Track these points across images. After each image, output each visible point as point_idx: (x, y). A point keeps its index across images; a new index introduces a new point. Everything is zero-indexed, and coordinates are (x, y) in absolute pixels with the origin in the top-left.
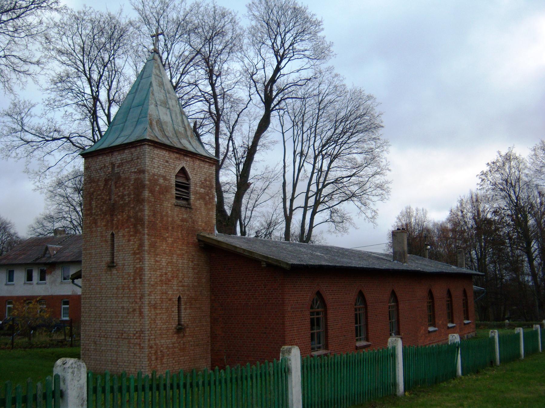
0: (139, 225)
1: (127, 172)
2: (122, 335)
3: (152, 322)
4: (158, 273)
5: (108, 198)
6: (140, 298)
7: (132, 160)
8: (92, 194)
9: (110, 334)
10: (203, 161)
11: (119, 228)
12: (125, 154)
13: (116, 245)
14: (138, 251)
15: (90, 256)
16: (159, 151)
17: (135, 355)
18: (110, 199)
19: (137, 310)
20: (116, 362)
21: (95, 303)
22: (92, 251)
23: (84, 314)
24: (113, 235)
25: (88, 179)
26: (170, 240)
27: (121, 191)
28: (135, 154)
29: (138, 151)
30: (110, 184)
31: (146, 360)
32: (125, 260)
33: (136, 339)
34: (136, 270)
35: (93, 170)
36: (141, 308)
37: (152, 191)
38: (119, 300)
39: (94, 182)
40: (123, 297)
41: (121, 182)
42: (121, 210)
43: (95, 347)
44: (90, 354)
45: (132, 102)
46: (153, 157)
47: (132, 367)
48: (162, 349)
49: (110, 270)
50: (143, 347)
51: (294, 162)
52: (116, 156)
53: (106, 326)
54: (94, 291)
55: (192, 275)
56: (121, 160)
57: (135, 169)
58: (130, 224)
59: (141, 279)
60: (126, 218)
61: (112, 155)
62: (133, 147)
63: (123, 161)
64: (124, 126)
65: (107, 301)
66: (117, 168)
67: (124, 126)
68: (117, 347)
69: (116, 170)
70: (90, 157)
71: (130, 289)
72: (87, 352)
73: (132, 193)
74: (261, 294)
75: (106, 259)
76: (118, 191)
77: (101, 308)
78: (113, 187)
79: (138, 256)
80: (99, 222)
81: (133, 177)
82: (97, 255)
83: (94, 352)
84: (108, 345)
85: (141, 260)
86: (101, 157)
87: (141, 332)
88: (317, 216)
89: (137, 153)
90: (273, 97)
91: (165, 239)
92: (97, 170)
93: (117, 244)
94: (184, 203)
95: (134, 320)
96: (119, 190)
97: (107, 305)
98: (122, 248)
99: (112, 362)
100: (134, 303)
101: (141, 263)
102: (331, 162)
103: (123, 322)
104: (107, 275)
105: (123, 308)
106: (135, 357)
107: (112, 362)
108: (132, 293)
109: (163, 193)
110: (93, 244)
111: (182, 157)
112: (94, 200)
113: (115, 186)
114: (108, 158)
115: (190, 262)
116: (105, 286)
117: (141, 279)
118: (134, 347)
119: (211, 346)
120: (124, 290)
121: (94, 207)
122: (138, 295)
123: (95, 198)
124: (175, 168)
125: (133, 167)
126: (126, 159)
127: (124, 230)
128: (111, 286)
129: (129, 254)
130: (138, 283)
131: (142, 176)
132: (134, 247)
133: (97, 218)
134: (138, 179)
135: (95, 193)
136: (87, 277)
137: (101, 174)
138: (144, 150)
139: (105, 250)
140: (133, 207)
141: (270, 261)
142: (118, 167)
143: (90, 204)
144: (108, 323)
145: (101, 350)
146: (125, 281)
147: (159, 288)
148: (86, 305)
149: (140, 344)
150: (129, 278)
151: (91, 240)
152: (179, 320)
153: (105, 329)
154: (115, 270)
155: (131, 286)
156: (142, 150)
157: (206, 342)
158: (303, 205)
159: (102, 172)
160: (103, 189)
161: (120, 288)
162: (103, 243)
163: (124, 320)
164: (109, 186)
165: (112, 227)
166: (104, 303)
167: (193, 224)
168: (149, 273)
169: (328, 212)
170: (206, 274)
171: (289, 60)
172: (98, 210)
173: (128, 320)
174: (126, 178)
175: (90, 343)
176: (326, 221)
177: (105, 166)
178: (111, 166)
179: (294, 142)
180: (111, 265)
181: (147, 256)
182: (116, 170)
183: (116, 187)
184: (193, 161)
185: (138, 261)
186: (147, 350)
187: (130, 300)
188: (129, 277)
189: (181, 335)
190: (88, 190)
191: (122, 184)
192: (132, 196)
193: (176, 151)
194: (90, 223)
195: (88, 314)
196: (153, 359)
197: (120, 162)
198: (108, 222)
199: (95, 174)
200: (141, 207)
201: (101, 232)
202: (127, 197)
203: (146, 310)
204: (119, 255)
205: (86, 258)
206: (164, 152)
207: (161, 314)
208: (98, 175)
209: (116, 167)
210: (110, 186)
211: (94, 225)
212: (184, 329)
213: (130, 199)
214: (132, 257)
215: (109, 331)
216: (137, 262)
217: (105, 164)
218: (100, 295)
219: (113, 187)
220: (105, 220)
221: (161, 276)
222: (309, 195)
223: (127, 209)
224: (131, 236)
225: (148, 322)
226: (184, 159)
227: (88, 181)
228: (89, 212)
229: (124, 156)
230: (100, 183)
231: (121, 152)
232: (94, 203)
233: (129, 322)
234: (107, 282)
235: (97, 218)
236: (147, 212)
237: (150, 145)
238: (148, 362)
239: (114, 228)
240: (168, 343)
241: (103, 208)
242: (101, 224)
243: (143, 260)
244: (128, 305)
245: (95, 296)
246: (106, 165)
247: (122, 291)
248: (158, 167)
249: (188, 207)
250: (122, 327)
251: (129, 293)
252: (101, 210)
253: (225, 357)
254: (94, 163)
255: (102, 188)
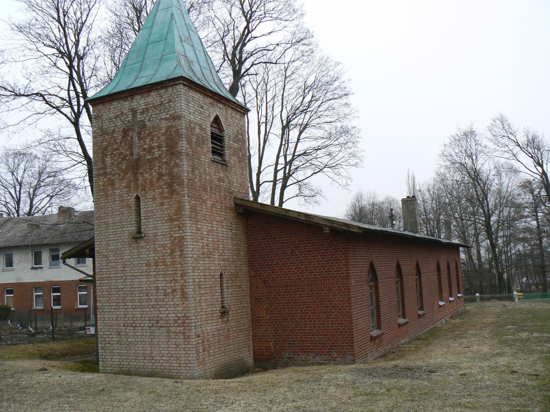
0: (175, 185)
1: (154, 119)
2: (158, 323)
3: (198, 305)
4: (200, 244)
5: (128, 152)
6: (182, 276)
7: (162, 104)
8: (106, 148)
9: (140, 322)
10: (235, 110)
11: (147, 189)
12: (151, 97)
13: (143, 211)
14: (175, 217)
15: (106, 226)
16: (193, 93)
17: (177, 347)
18: (132, 154)
19: (178, 291)
20: (151, 356)
21: (117, 284)
22: (108, 220)
23: (100, 299)
24: (138, 198)
25: (98, 131)
26: (209, 203)
27: (148, 143)
28: (166, 96)
29: (170, 92)
30: (131, 135)
31: (194, 352)
32: (157, 229)
33: (178, 326)
34: (173, 241)
35: (105, 119)
36: (184, 287)
37: (189, 142)
38: (150, 280)
39: (108, 134)
40: (158, 274)
41: (147, 132)
42: (148, 167)
43: (118, 339)
44: (112, 348)
45: (149, 37)
46: (188, 99)
47: (175, 362)
48: (208, 337)
49: (137, 243)
50: (188, 336)
51: (259, 134)
52: (138, 100)
53: (134, 313)
54: (114, 269)
55: (231, 247)
56: (146, 105)
57: (167, 115)
58: (162, 184)
59: (182, 251)
60: (157, 176)
61: (132, 99)
62: (162, 88)
63: (148, 106)
64: (142, 66)
65: (134, 281)
66: (140, 115)
67: (142, 66)
68: (151, 337)
69: (139, 117)
70: (101, 103)
71: (166, 265)
72: (108, 345)
73: (164, 145)
74: (318, 267)
75: (128, 229)
76: (143, 144)
77: (125, 290)
78: (136, 139)
79: (176, 223)
80: (117, 183)
81: (164, 124)
82: (116, 224)
83: (118, 345)
84: (137, 335)
85: (181, 228)
86: (115, 103)
87: (184, 318)
88: (286, 191)
89: (169, 95)
90: (243, 60)
91: (204, 201)
92: (111, 119)
93: (145, 209)
94: (218, 158)
95: (173, 303)
96: (144, 142)
97: (134, 286)
98: (152, 214)
99: (145, 357)
100: (174, 282)
101: (181, 232)
102: (301, 133)
103: (158, 306)
104: (131, 248)
105: (157, 288)
106: (179, 349)
107: (145, 357)
108: (170, 269)
109: (199, 146)
110: (110, 211)
111: (215, 103)
112: (108, 156)
113: (139, 137)
114: (127, 103)
115: (229, 231)
116: (129, 263)
117: (182, 251)
118: (176, 337)
119: (253, 331)
120: (157, 266)
121: (108, 165)
122: (178, 272)
123: (109, 153)
124: (209, 116)
125: (163, 113)
126: (153, 103)
127: (154, 191)
128: (138, 262)
129: (163, 222)
130: (177, 257)
131: (177, 122)
132: (169, 212)
133: (114, 178)
134: (172, 127)
135: (110, 148)
136: (102, 252)
137: (117, 124)
138: (178, 90)
139: (127, 217)
140: (166, 163)
141: (335, 226)
142: (142, 113)
143: (103, 161)
144: (136, 308)
145: (127, 343)
146: (158, 255)
147: (201, 262)
148: (103, 287)
149: (184, 333)
150: (164, 252)
151: (106, 207)
152: (222, 302)
153: (132, 316)
154: (143, 242)
155: (167, 260)
156: (175, 91)
157: (248, 326)
158: (272, 179)
159: (119, 121)
160: (121, 143)
161: (153, 264)
162: (125, 209)
163: (160, 303)
164: (129, 138)
165: (137, 189)
166: (129, 283)
167: (229, 185)
168: (191, 243)
169: (296, 187)
170: (244, 245)
171: (260, 22)
172: (115, 169)
173: (164, 303)
174: (154, 127)
175: (111, 335)
176: (297, 196)
177: (122, 114)
178: (131, 113)
179: (258, 113)
180: (138, 236)
181: (188, 223)
182: (139, 117)
183: (140, 139)
184: (226, 109)
185: (177, 229)
186: (194, 340)
187: (167, 279)
188: (164, 249)
189: (225, 319)
190: (99, 145)
191: (149, 135)
192: (164, 149)
193: (210, 95)
194: (103, 185)
195: (106, 299)
196: (201, 351)
197: (144, 107)
198: (130, 182)
199: (108, 123)
200: (177, 161)
201: (121, 196)
202: (156, 150)
203: (190, 291)
204: (148, 223)
205: (99, 229)
206: (199, 95)
207: (206, 295)
208: (113, 125)
209: (138, 114)
210: (132, 138)
211: (109, 188)
212: (228, 312)
213: (160, 152)
214: (167, 224)
215: (139, 319)
216: (175, 231)
217: (122, 112)
218: (123, 275)
219: (136, 139)
220: (125, 180)
221: (203, 247)
222: (278, 168)
223: (157, 165)
224: (165, 198)
225: (193, 305)
226: (217, 106)
227: (98, 133)
228: (101, 172)
229: (150, 99)
230: (116, 135)
231: (145, 95)
232: (108, 160)
233: (168, 306)
234: (133, 257)
235: (114, 178)
236: (185, 168)
237: (185, 85)
238: (196, 355)
239: (139, 190)
240: (213, 330)
241: (122, 166)
242: (121, 186)
243: (184, 228)
244: (164, 285)
245: (115, 275)
246: (124, 112)
247: (155, 267)
248: (194, 113)
249: (224, 164)
250: (157, 312)
251: (165, 270)
252: (120, 169)
253: (271, 344)
254: (106, 111)
255: (119, 141)
